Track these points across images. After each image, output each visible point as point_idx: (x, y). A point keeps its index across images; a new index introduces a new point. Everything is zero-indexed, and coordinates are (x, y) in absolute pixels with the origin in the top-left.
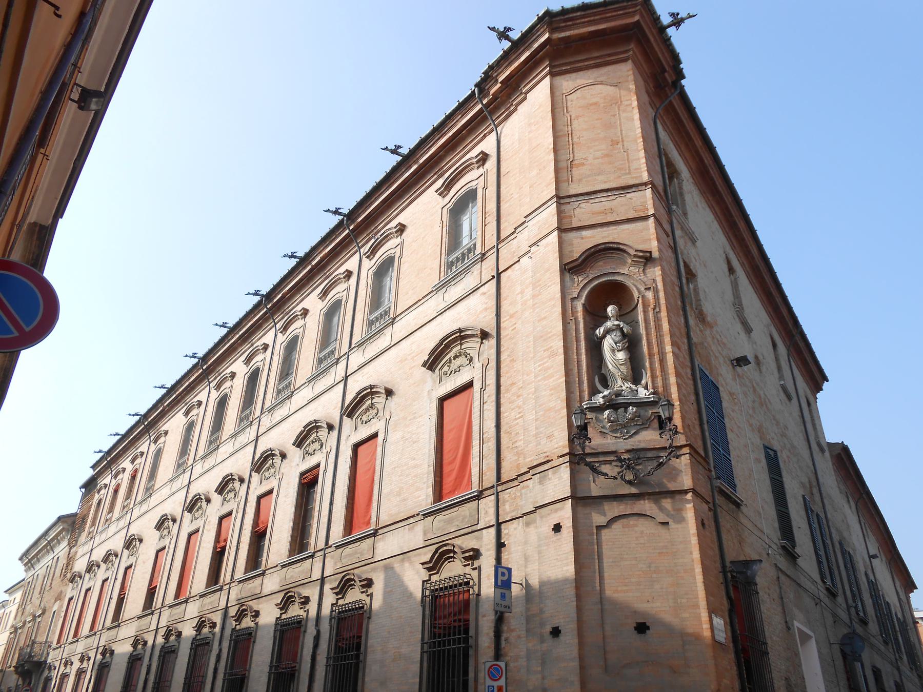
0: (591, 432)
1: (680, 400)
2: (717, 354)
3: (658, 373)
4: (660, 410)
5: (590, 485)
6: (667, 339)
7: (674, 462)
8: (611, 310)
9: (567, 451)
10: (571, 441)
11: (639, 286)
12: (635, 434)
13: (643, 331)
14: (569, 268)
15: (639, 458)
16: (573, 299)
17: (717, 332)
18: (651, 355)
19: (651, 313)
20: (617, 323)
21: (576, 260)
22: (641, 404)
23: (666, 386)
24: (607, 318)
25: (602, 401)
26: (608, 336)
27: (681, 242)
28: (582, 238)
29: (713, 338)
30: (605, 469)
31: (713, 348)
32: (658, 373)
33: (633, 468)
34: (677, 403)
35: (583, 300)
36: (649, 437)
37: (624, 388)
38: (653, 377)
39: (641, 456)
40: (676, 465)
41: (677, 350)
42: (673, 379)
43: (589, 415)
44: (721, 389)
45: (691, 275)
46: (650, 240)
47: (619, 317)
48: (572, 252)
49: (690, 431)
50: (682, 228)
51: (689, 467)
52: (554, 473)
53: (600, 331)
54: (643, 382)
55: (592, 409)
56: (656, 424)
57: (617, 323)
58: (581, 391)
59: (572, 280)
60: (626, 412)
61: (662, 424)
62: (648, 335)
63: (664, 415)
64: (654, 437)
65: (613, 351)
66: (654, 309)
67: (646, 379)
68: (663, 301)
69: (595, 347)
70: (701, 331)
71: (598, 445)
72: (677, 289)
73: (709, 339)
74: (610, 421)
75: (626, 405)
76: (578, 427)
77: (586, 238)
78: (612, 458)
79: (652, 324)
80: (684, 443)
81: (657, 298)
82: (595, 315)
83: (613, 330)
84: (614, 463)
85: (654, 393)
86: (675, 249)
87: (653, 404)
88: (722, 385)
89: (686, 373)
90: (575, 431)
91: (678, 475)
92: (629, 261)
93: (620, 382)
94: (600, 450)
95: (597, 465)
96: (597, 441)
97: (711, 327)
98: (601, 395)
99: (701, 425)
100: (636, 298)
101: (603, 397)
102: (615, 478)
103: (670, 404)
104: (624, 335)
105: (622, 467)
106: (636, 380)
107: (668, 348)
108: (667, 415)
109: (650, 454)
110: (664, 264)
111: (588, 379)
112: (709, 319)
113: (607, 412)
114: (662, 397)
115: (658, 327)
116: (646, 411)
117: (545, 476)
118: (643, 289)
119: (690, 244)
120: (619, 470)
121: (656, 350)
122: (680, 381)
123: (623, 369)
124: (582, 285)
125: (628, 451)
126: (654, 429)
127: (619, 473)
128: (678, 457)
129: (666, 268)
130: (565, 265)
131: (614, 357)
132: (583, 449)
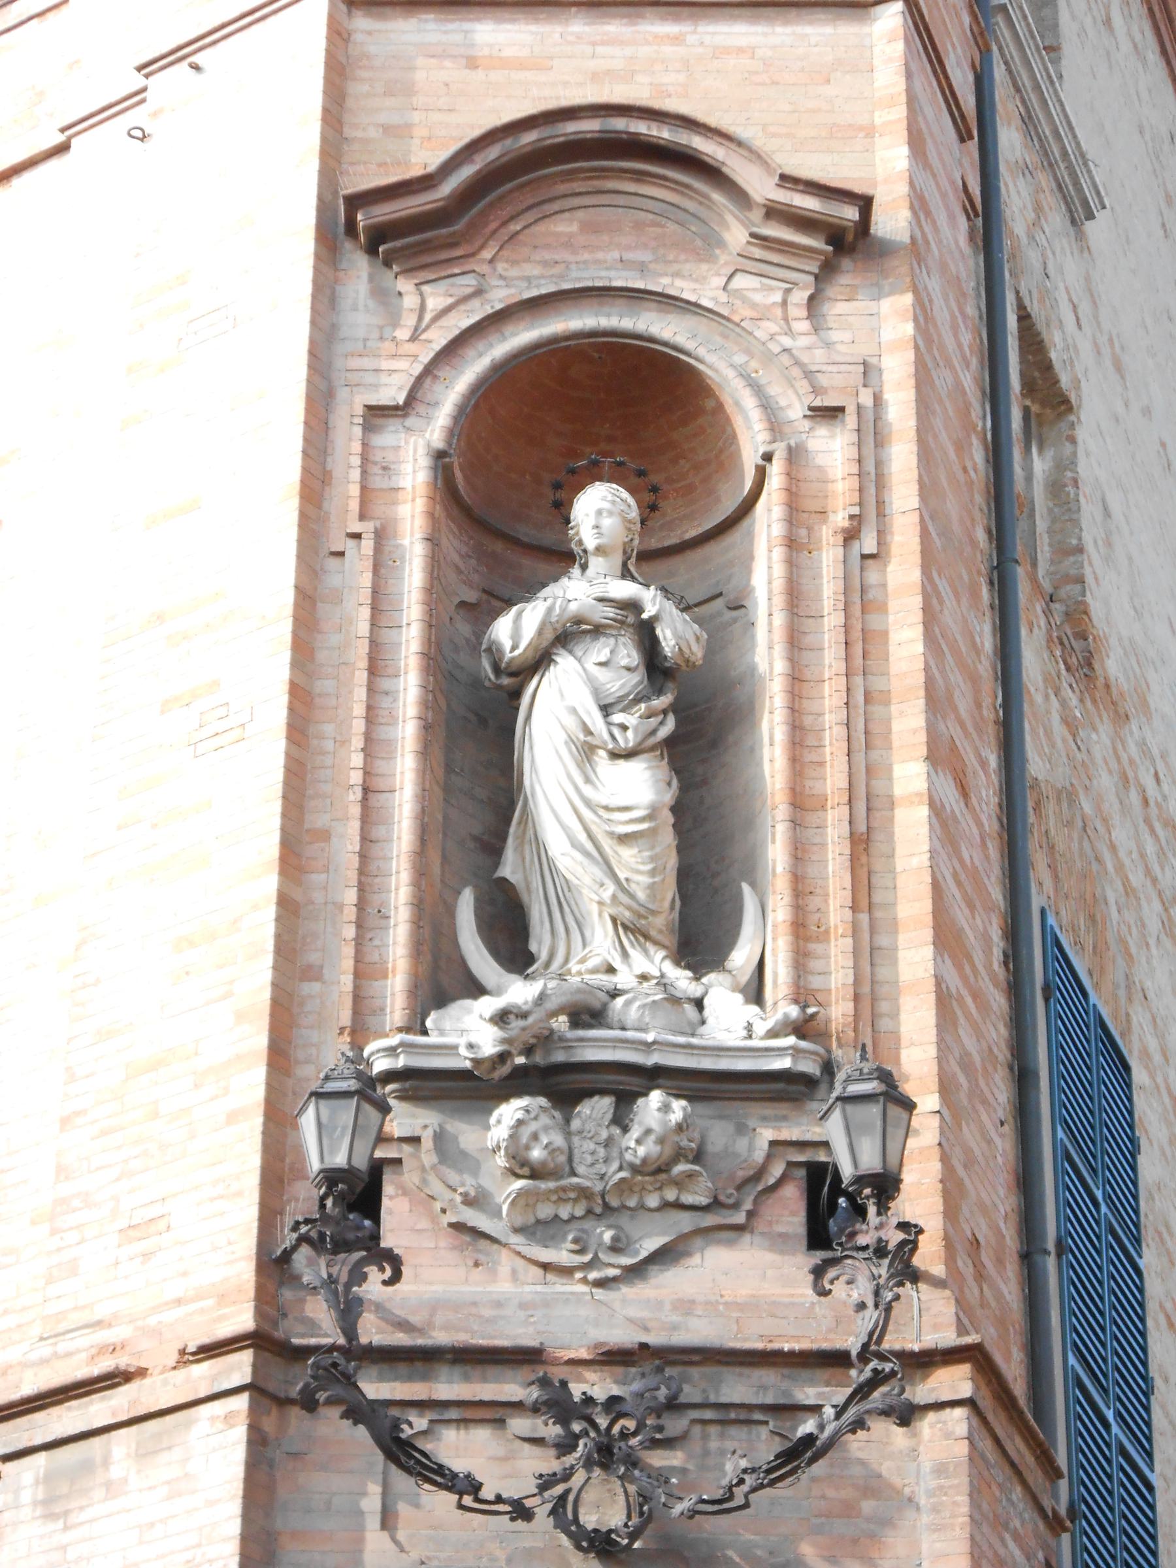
0: (399, 1220)
1: (946, 1088)
2: (1137, 878)
3: (836, 910)
4: (834, 1129)
5: (359, 1540)
6: (908, 722)
7: (881, 1445)
8: (599, 511)
9: (243, 1320)
10: (274, 1267)
11: (775, 390)
12: (664, 1256)
13: (767, 655)
14: (384, 228)
15: (673, 1405)
16: (377, 414)
17: (1143, 745)
18: (802, 804)
19: (829, 559)
20: (625, 589)
21: (427, 182)
22: (708, 1086)
23: (870, 996)
24: (564, 558)
25: (488, 1041)
26: (565, 665)
27: (1016, 197)
28: (472, 63)
29: (1125, 779)
30: (459, 1449)
31: (1121, 835)
32: (836, 910)
33: (633, 1462)
34: (928, 1102)
35: (436, 426)
36: (748, 1287)
37: (624, 978)
38: (804, 932)
39: (690, 1394)
40: (886, 1469)
41: (949, 794)
42: (915, 960)
43: (404, 1119)
44: (1139, 1075)
45: (1051, 401)
46: (870, 131)
47: (643, 559)
48: (398, 132)
49: (980, 1275)
50: (1028, 121)
51: (961, 1480)
52: (143, 1454)
53: (515, 629)
54: (741, 957)
55: (423, 1084)
56: (789, 1211)
57: (625, 589)
58: (366, 972)
59: (385, 298)
60: (621, 1121)
61: (833, 1210)
62: (798, 682)
63: (851, 1154)
64: (772, 1290)
65: (586, 751)
66: (850, 536)
67: (762, 934)
68: (904, 497)
69: (479, 721)
70: (1069, 723)
71: (435, 1306)
72: (978, 455)
73: (1105, 782)
74: (521, 1166)
75: (627, 1083)
76: (331, 1177)
77: (505, 64)
78: (511, 1387)
79: (831, 620)
80: (948, 1338)
81: (872, 479)
82: (499, 521)
83: (598, 631)
84: (520, 1424)
85: (802, 1028)
86: (985, 215)
87: (790, 1089)
88: (1145, 1054)
89: (986, 938)
90: (304, 1198)
91: (886, 1522)
92: (736, 235)
93: (602, 942)
94: (441, 1338)
95: (420, 1422)
96: (442, 1278)
97: (1121, 718)
98: (488, 1005)
99: (1029, 1257)
100: (750, 458)
101: (501, 1018)
102: (521, 1511)
103: (893, 1097)
104: (656, 668)
105: (565, 1446)
106: (700, 936)
107: (909, 775)
108: (870, 1162)
109: (738, 1388)
110: (934, 285)
111: (419, 905)
112: (1112, 665)
113: (510, 1111)
114: (846, 1059)
115: (863, 644)
116: (741, 1129)
117: (87, 1467)
118: (795, 410)
119: (1056, 219)
120: (548, 1463)
121: (833, 778)
122: (953, 981)
123: (633, 864)
124: (439, 338)
125: (614, 1358)
126: (779, 1242)
127: (546, 1483)
128: (906, 1415)
129: (941, 312)
130: (356, 202)
131: (587, 790)
132: (349, 1311)
